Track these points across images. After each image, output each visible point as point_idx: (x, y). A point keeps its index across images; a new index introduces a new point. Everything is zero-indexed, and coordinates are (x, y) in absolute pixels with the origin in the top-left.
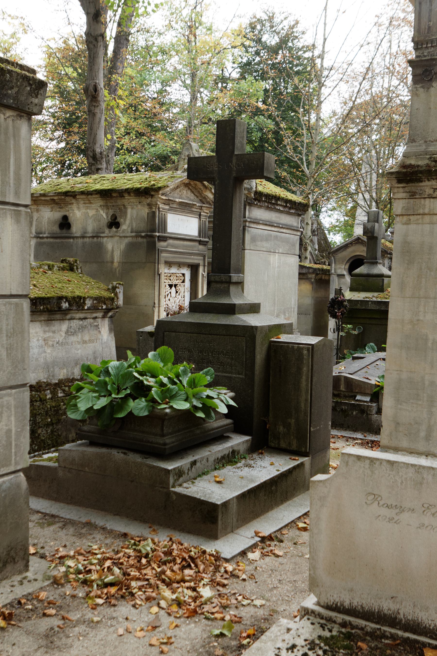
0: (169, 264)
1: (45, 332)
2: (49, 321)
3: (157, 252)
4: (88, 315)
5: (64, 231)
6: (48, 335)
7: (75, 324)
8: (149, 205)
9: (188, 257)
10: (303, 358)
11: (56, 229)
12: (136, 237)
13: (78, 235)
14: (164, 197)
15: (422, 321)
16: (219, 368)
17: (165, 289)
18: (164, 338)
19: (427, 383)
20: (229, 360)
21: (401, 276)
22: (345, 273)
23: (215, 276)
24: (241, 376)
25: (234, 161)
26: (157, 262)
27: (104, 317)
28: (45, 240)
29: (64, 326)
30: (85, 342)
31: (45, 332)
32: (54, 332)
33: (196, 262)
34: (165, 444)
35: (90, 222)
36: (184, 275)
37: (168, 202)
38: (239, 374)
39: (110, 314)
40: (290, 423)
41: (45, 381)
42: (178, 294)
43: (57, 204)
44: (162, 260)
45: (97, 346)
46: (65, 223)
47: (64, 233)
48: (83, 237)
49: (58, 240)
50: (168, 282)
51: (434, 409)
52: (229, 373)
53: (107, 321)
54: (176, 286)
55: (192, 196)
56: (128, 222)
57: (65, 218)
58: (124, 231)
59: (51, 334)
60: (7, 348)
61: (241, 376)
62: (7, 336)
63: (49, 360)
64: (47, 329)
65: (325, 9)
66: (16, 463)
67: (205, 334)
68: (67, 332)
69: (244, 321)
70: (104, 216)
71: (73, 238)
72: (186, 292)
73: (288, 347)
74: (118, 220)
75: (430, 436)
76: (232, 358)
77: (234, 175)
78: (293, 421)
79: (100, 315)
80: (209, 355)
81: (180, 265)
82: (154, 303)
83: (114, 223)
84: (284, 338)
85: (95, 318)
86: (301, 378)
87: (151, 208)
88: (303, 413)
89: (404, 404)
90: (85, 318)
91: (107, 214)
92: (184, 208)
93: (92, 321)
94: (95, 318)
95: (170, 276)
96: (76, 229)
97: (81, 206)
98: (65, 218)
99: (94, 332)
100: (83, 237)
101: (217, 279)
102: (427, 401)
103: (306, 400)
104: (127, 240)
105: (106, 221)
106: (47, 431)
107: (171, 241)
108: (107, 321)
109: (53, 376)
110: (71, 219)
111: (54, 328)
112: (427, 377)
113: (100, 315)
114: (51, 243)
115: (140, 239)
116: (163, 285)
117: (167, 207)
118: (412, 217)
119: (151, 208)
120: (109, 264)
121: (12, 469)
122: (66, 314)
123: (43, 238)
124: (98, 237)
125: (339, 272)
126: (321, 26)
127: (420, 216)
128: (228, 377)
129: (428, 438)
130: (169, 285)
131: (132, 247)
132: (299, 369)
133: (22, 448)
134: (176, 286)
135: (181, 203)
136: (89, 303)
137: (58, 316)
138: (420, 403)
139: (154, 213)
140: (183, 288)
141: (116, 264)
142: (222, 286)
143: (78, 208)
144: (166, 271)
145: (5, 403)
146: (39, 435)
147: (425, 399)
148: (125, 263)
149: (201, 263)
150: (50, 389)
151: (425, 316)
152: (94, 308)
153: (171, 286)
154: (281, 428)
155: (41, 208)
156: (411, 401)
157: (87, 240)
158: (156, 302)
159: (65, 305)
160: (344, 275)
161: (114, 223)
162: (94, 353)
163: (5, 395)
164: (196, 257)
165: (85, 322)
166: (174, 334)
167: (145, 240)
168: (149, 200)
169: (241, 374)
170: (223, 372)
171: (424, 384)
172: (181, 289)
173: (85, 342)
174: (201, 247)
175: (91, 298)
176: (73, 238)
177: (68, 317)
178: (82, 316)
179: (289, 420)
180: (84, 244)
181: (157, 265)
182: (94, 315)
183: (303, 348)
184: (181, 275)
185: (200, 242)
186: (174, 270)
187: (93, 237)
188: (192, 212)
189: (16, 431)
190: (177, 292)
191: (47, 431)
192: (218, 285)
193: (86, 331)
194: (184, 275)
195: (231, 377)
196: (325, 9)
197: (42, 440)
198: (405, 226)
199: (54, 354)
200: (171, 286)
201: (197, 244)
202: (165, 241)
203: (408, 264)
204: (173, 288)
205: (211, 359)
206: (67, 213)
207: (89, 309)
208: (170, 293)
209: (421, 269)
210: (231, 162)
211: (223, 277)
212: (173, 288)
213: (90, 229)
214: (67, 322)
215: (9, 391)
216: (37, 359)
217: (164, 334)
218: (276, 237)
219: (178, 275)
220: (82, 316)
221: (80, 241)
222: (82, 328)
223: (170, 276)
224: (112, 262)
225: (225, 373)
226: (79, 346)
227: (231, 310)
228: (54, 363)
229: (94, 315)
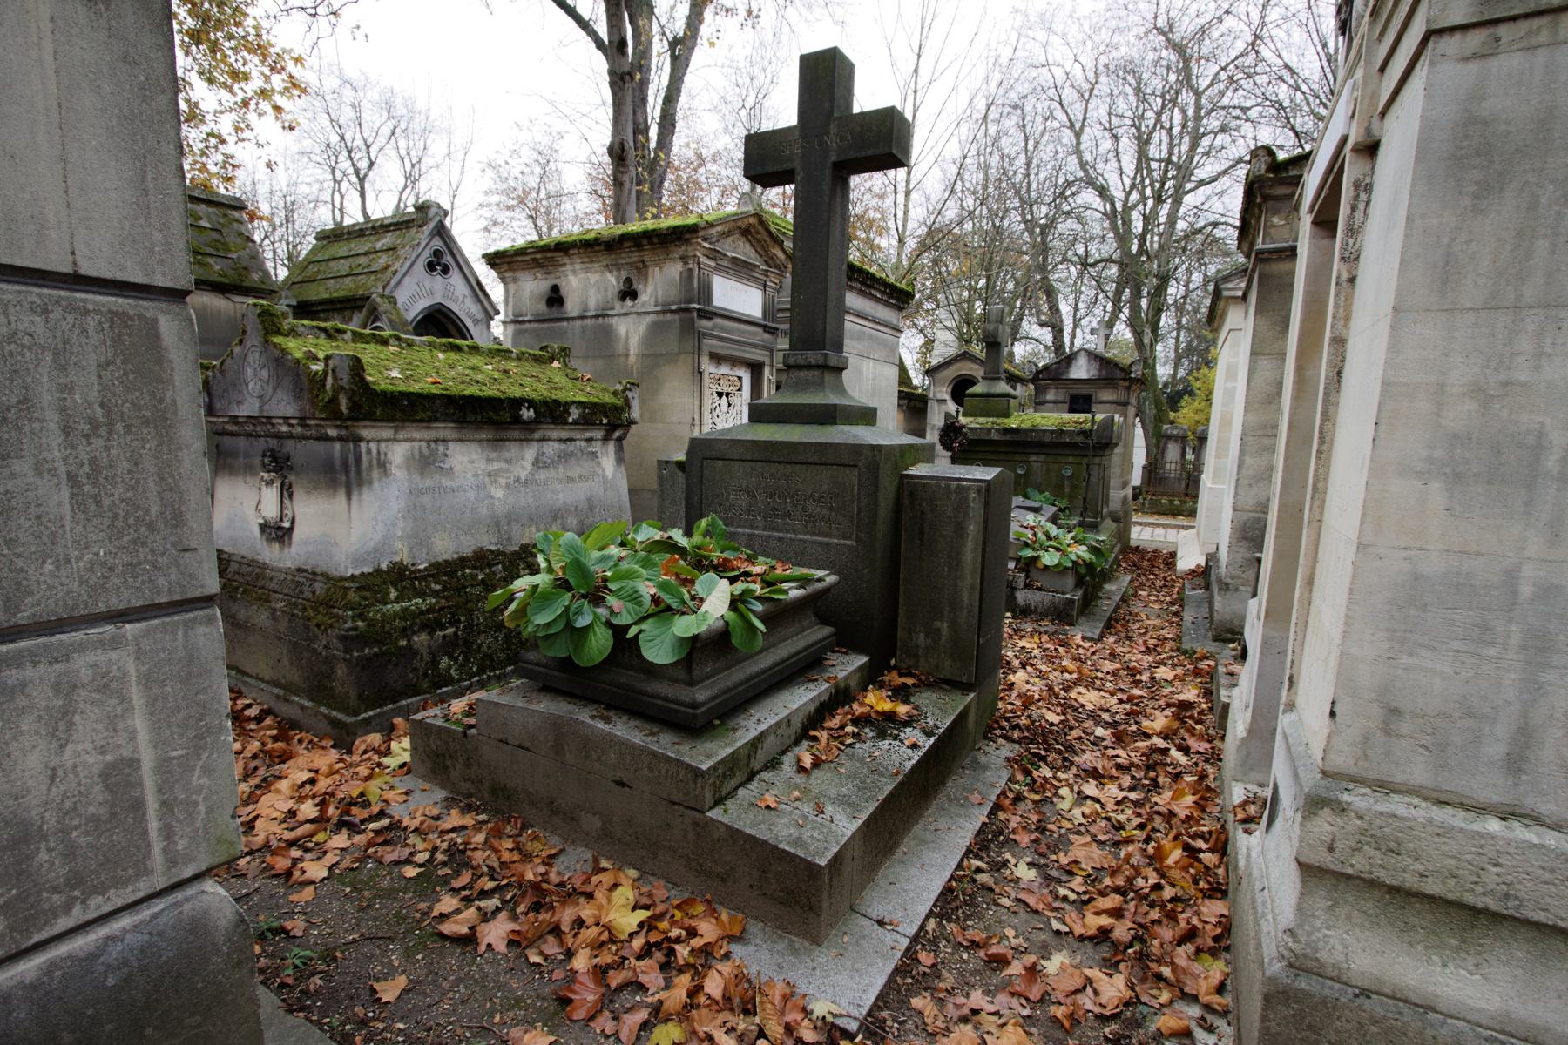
0: (717, 358)
1: (489, 460)
2: (498, 441)
4: (577, 435)
5: (554, 309)
6: (495, 466)
7: (551, 448)
8: (682, 258)
10: (968, 507)
11: (542, 307)
12: (663, 312)
13: (575, 314)
14: (706, 245)
15: (1524, 385)
17: (710, 399)
19: (1526, 590)
20: (825, 511)
21: (1446, 240)
22: (947, 397)
24: (848, 542)
25: (833, 129)
27: (606, 438)
28: (527, 326)
29: (530, 452)
30: (570, 480)
31: (489, 460)
32: (509, 461)
33: (760, 358)
34: (695, 705)
35: (592, 292)
36: (740, 378)
37: (715, 255)
39: (617, 434)
41: (493, 548)
43: (542, 267)
44: (706, 350)
45: (594, 487)
46: (555, 298)
47: (555, 312)
48: (582, 317)
49: (546, 325)
50: (715, 388)
51: (1548, 676)
53: (611, 446)
54: (728, 395)
55: (752, 253)
56: (649, 289)
57: (555, 289)
58: (643, 305)
59: (504, 465)
60: (71, 477)
61: (848, 542)
62: (66, 430)
63: (500, 509)
64: (494, 455)
65: (916, 71)
66: (172, 861)
68: (536, 462)
69: (855, 436)
70: (613, 281)
71: (568, 319)
73: (938, 486)
74: (635, 286)
75: (1524, 759)
77: (834, 158)
79: (599, 434)
81: (735, 362)
83: (629, 293)
84: (919, 470)
85: (591, 439)
87: (686, 263)
89: (1424, 652)
90: (571, 440)
91: (617, 278)
92: (740, 269)
93: (583, 444)
94: (591, 439)
96: (572, 307)
97: (578, 267)
98: (555, 289)
99: (588, 465)
100: (582, 317)
101: (801, 361)
102: (1524, 648)
103: (972, 587)
104: (648, 319)
105: (617, 290)
106: (496, 638)
107: (718, 321)
108: (611, 446)
109: (509, 539)
110: (565, 291)
111: (508, 455)
112: (1528, 571)
113: (599, 434)
114: (535, 330)
115: (669, 316)
116: (707, 392)
117: (712, 263)
118: (1503, 31)
119: (686, 263)
120: (622, 359)
121: (160, 882)
122: (533, 431)
123: (523, 322)
124: (604, 316)
125: (939, 396)
126: (910, 92)
127: (1544, 20)
129: (1516, 763)
131: (656, 330)
132: (960, 529)
133: (202, 808)
134: (728, 395)
135: (735, 260)
136: (575, 413)
137: (516, 434)
138: (1492, 652)
139: (690, 271)
141: (632, 359)
143: (574, 272)
144: (712, 370)
145: (85, 674)
146: (480, 646)
147: (1514, 641)
148: (647, 356)
149: (767, 361)
150: (503, 563)
151: (1537, 368)
152: (586, 421)
153: (720, 395)
154: (922, 637)
155: (519, 275)
156: (1455, 645)
157: (588, 322)
158: (697, 417)
159: (527, 414)
161: (629, 293)
162: (589, 500)
163: (81, 648)
165: (571, 447)
166: (720, 463)
167: (677, 317)
168: (682, 250)
169: (850, 538)
170: (813, 534)
171: (1515, 593)
172: (735, 399)
173: (570, 480)
174: (767, 336)
175: (580, 403)
176: (568, 319)
177: (537, 435)
178: (564, 435)
179: (938, 624)
180: (583, 328)
182: (588, 435)
183: (968, 488)
185: (766, 329)
186: (724, 370)
187: (597, 317)
188: (753, 279)
189: (164, 767)
191: (496, 638)
192: (802, 374)
193: (573, 461)
194: (740, 378)
195: (828, 544)
196: (916, 71)
197: (486, 655)
198: (1474, 66)
199: (511, 500)
200: (720, 395)
201: (760, 330)
203: (1476, 196)
206: (557, 282)
207: (575, 423)
209: (1533, 206)
210: (827, 134)
211: (813, 357)
213: (592, 304)
214: (536, 444)
215: (108, 629)
216: (474, 510)
218: (871, 336)
220: (564, 435)
221: (578, 323)
222: (564, 457)
224: (627, 356)
226: (559, 487)
227: (828, 415)
228: (511, 517)
229: (588, 435)
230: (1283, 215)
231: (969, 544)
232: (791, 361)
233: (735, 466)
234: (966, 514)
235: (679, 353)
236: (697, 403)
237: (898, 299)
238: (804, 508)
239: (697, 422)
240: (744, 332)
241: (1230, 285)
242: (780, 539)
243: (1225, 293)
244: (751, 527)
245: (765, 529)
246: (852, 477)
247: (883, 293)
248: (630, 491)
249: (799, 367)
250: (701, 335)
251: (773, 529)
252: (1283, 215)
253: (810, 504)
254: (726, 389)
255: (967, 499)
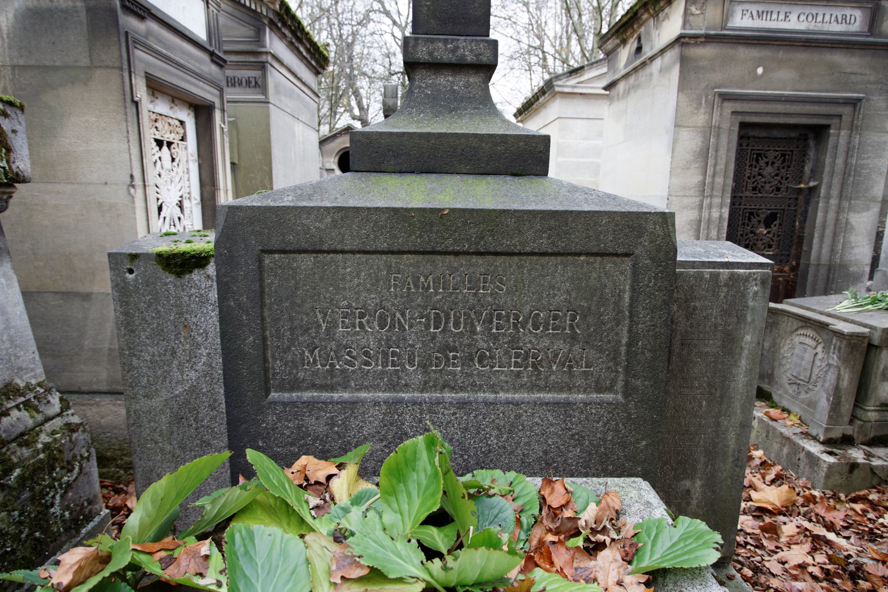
0: (156, 87)
3: (123, 40)
9: (188, 77)
16: (518, 375)
18: (261, 280)
22: (335, 167)
23: (432, 41)
24: (608, 397)
26: (126, 67)
38: (599, 390)
40: (688, 492)
42: (175, 164)
52: (561, 390)
54: (169, 144)
67: (456, 254)
72: (191, 163)
73: (700, 276)
76: (574, 337)
78: (699, 483)
80: (474, 332)
81: (177, 96)
82: (132, 176)
86: (736, 364)
88: (731, 460)
95: (156, 121)
107: (154, 26)
128: (557, 404)
130: (156, 140)
132: (730, 342)
134: (169, 144)
140: (184, 152)
142: (459, 82)
160: (333, 170)
164: (207, 87)
166: (306, 262)
169: (610, 389)
170: (533, 387)
174: (214, 68)
179: (687, 483)
181: (126, 75)
183: (747, 279)
184: (178, 123)
186: (162, 107)
190: (173, 160)
192: (444, 80)
194: (182, 123)
195: (568, 404)
200: (160, 143)
201: (205, 57)
202: (142, 18)
204: (165, 148)
205: (482, 344)
208: (160, 158)
212: (165, 148)
217: (260, 261)
218: (298, 95)
219: (172, 122)
223: (156, 121)
225: (541, 389)
230: (699, 5)
231: (743, 363)
232: (422, 53)
233: (348, 265)
234: (741, 318)
235: (91, 68)
236: (135, 151)
237: (317, 62)
238: (514, 341)
239: (138, 181)
240: (188, 54)
241: (559, 83)
242: (462, 405)
243: (557, 89)
244: (393, 387)
245: (424, 387)
246: (619, 276)
247: (308, 51)
248: (27, 295)
249: (436, 67)
250: (130, 41)
251: (445, 386)
252: (699, 5)
253: (528, 339)
254: (167, 137)
255: (744, 296)
